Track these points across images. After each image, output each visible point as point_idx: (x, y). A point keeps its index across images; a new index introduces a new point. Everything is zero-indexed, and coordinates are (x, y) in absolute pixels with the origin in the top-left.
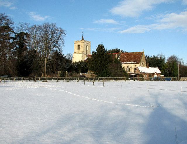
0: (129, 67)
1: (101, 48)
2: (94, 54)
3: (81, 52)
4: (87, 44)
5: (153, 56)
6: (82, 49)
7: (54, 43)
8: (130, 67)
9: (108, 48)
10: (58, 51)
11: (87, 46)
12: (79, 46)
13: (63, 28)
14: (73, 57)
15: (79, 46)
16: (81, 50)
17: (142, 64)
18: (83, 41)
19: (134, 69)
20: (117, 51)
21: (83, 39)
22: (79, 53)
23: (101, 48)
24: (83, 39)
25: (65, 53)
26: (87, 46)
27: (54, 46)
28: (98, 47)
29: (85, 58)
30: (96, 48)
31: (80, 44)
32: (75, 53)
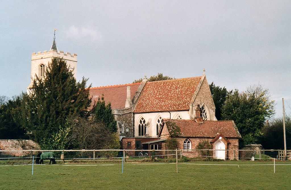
0: (144, 122)
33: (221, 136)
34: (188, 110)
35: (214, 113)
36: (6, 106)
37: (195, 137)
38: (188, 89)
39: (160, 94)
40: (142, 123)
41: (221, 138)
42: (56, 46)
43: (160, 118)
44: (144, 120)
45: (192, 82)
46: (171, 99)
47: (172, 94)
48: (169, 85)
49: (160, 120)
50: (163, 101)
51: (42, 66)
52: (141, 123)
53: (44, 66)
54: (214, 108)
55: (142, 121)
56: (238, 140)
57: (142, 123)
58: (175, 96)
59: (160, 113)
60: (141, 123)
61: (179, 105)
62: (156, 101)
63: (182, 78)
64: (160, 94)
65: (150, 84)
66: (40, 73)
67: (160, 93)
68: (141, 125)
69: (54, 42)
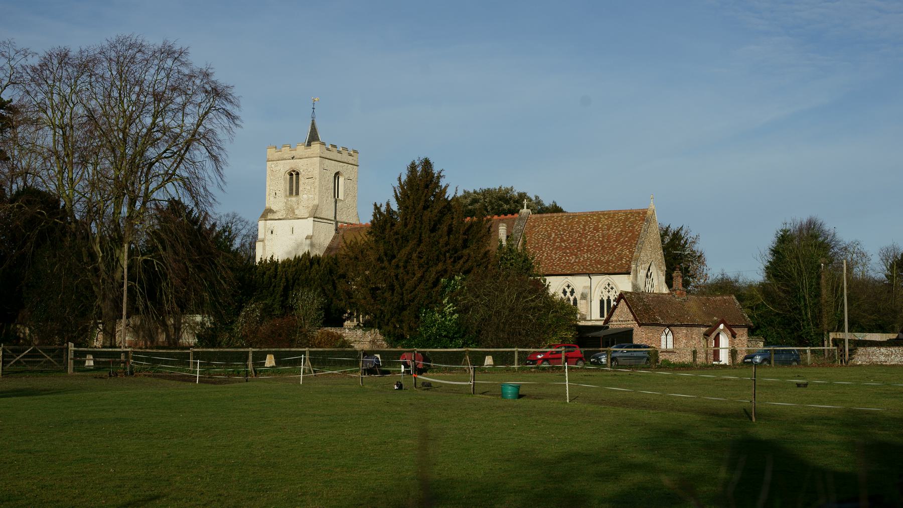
0: (572, 292)
1: (421, 184)
2: (383, 221)
3: (301, 211)
4: (339, 167)
5: (819, 222)
6: (309, 195)
7: (168, 163)
8: (577, 295)
9: (458, 182)
10: (187, 201)
11: (337, 174)
12: (294, 175)
13: (220, 78)
14: (260, 236)
15: (294, 175)
16: (303, 196)
17: (642, 273)
18: (316, 146)
19: (602, 302)
20: (505, 203)
21: (313, 137)
22: (291, 214)
23: (421, 184)
24: (313, 137)
25: (221, 209)
26: (337, 174)
27: (169, 177)
28: (404, 178)
29: (326, 236)
30: (397, 184)
31: (300, 165)
32: (270, 216)
33: (723, 322)
34: (629, 273)
35: (664, 278)
36: (228, 249)
37: (682, 325)
38: (622, 231)
39: (562, 241)
40: (568, 294)
41: (722, 326)
42: (316, 134)
43: (568, 286)
44: (573, 290)
45: (627, 219)
46: (588, 251)
47: (589, 241)
48: (578, 222)
49: (568, 291)
50: (572, 254)
51: (291, 175)
52: (565, 295)
53: (298, 174)
54: (664, 268)
55: (568, 291)
56: (636, 341)
57: (568, 294)
58: (597, 246)
59: (570, 277)
60: (565, 295)
61: (608, 262)
62: (556, 254)
63: (485, 187)
64: (562, 241)
65: (537, 218)
66: (288, 188)
67: (562, 238)
68: (605, 299)
69: (313, 124)
